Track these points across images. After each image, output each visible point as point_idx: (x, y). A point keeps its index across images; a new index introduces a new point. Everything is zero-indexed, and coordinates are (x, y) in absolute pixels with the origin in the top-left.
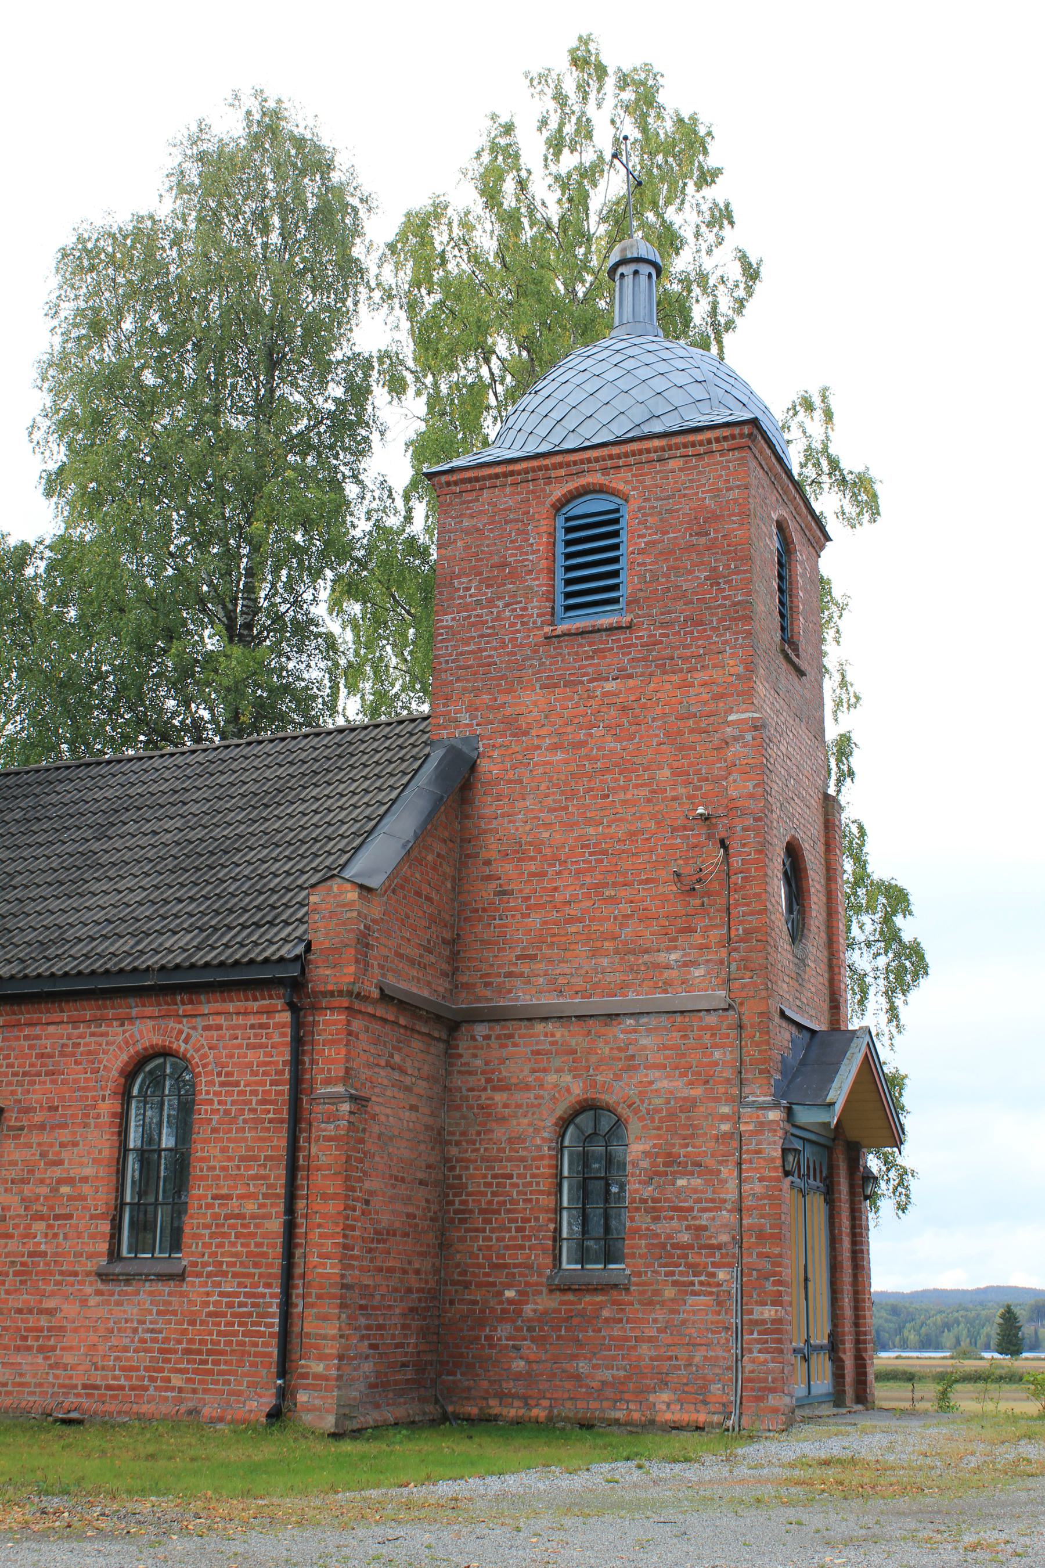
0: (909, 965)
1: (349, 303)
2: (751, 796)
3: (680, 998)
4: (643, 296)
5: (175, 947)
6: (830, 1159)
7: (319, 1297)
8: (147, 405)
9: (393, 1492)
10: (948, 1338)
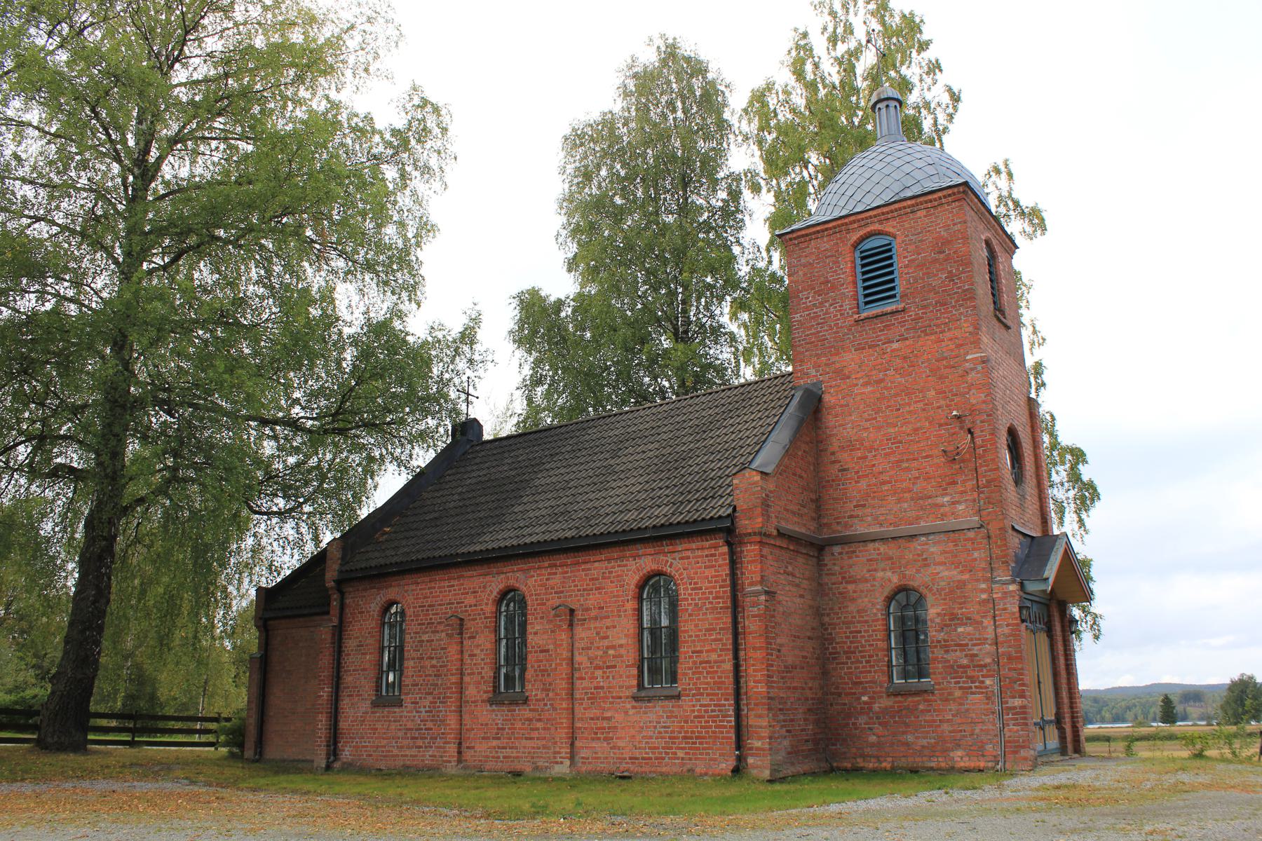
0: (1087, 494)
1: (725, 145)
2: (984, 402)
3: (951, 523)
4: (893, 120)
5: (661, 514)
6: (1049, 611)
7: (756, 705)
8: (618, 215)
9: (805, 810)
10: (1129, 715)
